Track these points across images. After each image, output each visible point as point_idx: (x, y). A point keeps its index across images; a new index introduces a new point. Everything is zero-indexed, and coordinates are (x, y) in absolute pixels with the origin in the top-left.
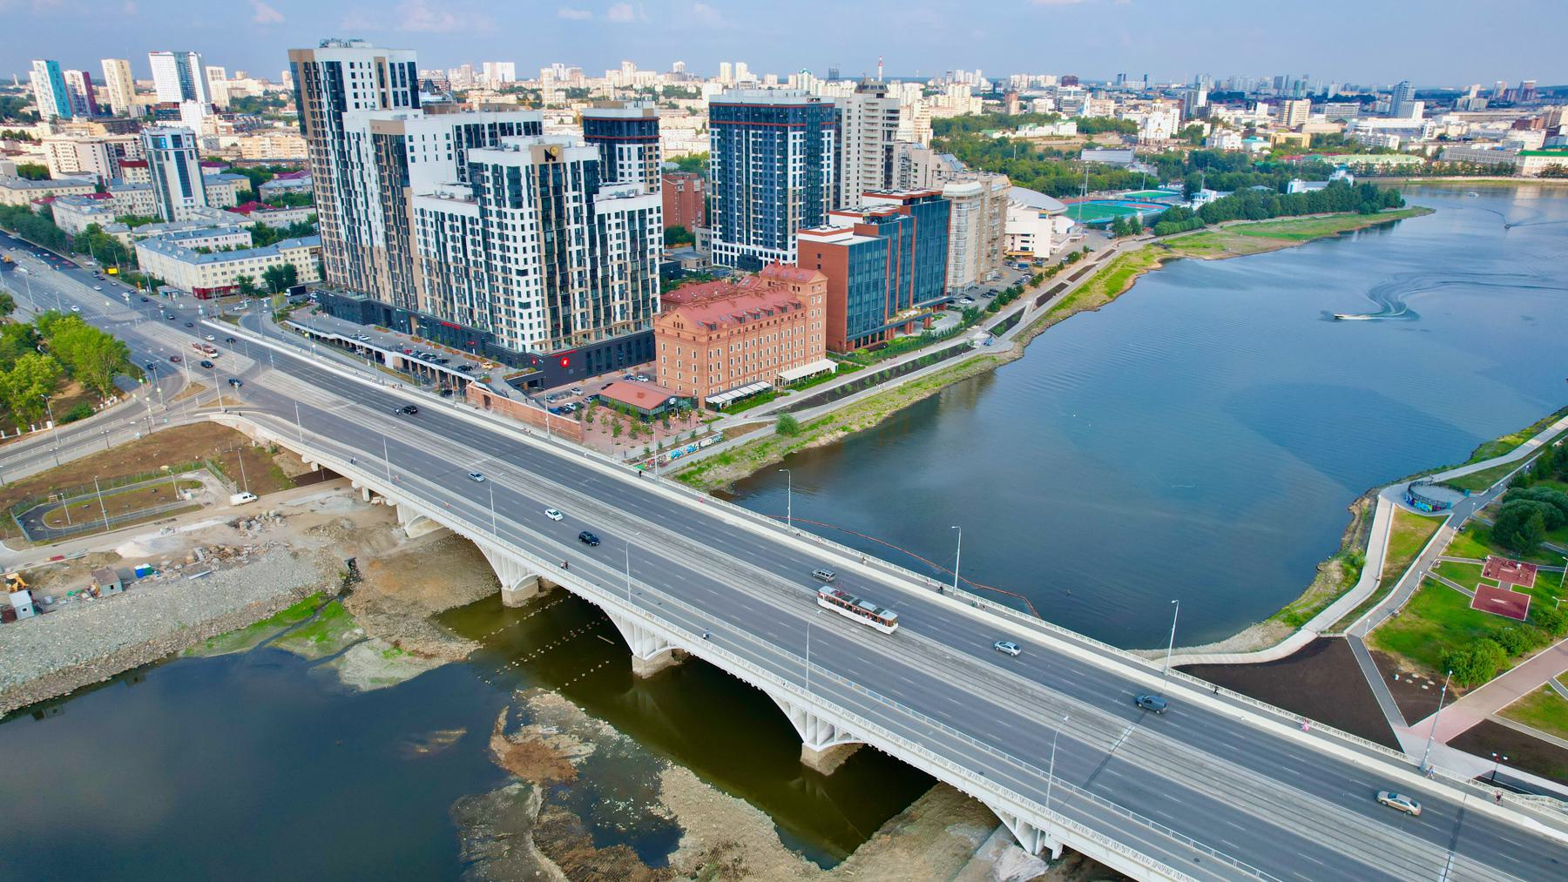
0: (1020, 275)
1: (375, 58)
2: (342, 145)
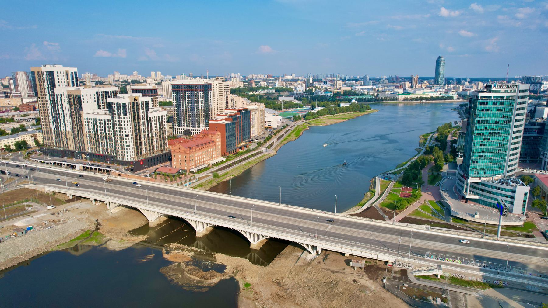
0: (270, 133)
1: (65, 70)
2: (54, 98)
